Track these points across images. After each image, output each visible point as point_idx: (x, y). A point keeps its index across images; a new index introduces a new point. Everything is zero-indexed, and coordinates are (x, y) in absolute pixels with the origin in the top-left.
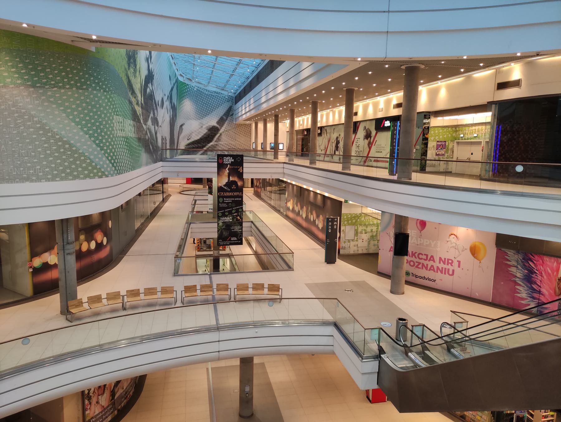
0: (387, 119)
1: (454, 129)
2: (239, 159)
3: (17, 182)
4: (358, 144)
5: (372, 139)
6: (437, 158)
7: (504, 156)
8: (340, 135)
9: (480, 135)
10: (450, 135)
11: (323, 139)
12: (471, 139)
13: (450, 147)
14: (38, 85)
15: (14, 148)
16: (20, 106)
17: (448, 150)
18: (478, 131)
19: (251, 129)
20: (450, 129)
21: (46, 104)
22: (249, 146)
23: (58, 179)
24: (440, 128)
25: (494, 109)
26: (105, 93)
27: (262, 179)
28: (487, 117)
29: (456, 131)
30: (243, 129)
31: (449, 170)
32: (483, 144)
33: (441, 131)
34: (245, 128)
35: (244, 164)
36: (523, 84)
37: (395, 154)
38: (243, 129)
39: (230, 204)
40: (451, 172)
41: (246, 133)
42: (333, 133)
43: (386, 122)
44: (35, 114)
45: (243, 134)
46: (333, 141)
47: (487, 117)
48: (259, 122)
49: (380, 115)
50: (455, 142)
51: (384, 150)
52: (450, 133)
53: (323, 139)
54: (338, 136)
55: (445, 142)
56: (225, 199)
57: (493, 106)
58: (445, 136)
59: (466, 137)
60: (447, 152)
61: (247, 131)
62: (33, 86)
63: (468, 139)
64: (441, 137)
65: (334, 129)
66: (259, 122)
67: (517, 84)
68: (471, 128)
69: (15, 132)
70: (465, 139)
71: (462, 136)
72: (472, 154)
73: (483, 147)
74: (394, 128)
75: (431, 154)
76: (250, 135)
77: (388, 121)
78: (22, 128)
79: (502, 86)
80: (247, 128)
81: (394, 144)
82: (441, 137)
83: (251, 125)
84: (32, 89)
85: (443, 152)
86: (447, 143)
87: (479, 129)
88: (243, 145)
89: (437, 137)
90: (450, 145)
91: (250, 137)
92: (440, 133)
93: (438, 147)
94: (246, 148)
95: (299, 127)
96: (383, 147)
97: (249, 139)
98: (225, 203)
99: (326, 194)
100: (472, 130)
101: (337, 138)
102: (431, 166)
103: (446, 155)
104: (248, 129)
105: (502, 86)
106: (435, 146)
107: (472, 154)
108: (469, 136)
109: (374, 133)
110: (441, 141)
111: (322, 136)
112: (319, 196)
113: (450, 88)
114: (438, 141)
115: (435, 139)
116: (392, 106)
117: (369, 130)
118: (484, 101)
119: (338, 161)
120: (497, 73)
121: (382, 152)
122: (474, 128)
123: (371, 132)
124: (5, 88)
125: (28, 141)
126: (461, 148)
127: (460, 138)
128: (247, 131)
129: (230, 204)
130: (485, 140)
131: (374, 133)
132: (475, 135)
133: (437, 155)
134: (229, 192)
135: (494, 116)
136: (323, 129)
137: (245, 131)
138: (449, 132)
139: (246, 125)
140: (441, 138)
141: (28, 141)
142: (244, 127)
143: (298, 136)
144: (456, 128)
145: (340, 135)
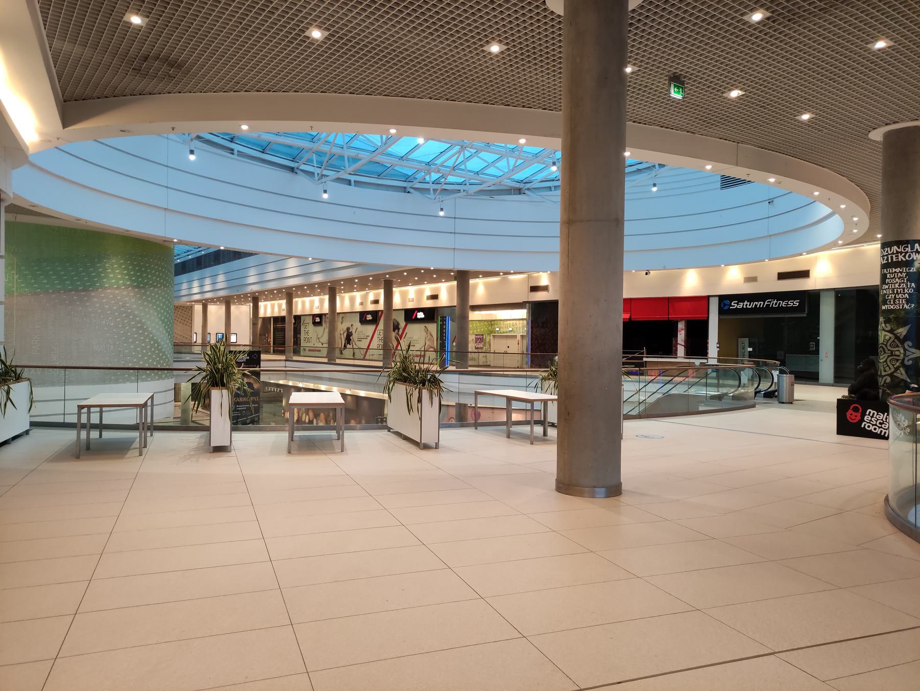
0: (420, 310)
1: (489, 322)
2: (256, 356)
3: (120, 383)
4: (307, 330)
5: (401, 331)
6: (476, 351)
7: (539, 349)
8: (352, 325)
9: (515, 329)
10: (486, 329)
11: (325, 329)
12: (506, 332)
13: (487, 340)
14: (141, 285)
15: (120, 348)
16: (127, 306)
17: (485, 343)
18: (513, 325)
19: (192, 314)
20: (486, 322)
21: (145, 303)
22: (189, 338)
23: (149, 379)
24: (477, 322)
25: (402, 185)
26: (166, 289)
27: (623, 349)
28: (523, 313)
29: (492, 325)
30: (179, 313)
31: (488, 364)
32: (519, 338)
33: (478, 324)
34: (183, 312)
35: (261, 362)
36: (550, 289)
37: (759, 361)
38: (179, 313)
39: (244, 412)
40: (490, 365)
41: (184, 318)
42: (342, 323)
43: (418, 314)
44: (137, 314)
45: (180, 320)
46: (342, 332)
47: (523, 313)
48: (209, 304)
49: (410, 306)
50: (491, 336)
51: (417, 343)
52: (486, 327)
53: (325, 329)
54: (350, 326)
55: (483, 335)
56: (237, 406)
57: (527, 304)
58: (482, 330)
59: (502, 330)
60: (485, 345)
61: (185, 316)
62: (138, 287)
63: (504, 333)
64: (479, 330)
65: (343, 318)
66: (209, 304)
67: (545, 288)
68: (505, 323)
69: (122, 332)
70: (501, 333)
71: (498, 329)
72: (508, 347)
73: (518, 341)
74: (443, 323)
75: (471, 347)
76: (190, 322)
77: (421, 313)
78: (127, 328)
79: (534, 289)
80: (185, 311)
81: (444, 338)
82: (479, 330)
83: (191, 307)
84: (137, 290)
85: (481, 345)
86: (484, 336)
87: (513, 323)
88: (178, 337)
89: (475, 331)
90: (487, 338)
91: (190, 325)
92: (477, 326)
93: (477, 340)
94: (185, 341)
95: (280, 311)
96: (416, 341)
97: (190, 328)
98: (238, 411)
99: (362, 393)
100: (507, 324)
101: (348, 329)
102: (472, 360)
103: (484, 348)
104: (187, 313)
105: (534, 289)
106: (474, 340)
107: (508, 347)
108: (505, 330)
109: (402, 324)
110: (479, 335)
111: (322, 325)
112: (349, 398)
113: (487, 286)
114: (476, 335)
115: (473, 332)
116: (425, 298)
117: (396, 321)
118: (520, 301)
119: (352, 357)
120: (529, 277)
121: (414, 346)
122: (508, 322)
123: (398, 324)
124: (118, 289)
125: (131, 340)
126: (497, 341)
127: (496, 332)
128: (185, 316)
129: (244, 412)
130: (520, 334)
131: (402, 324)
132: (511, 329)
133: (476, 348)
134: (243, 397)
135: (528, 313)
136: (324, 317)
137: (183, 317)
138: (485, 325)
139: (184, 307)
140: (479, 331)
141: (131, 340)
142: (180, 310)
143: (276, 324)
144: (492, 322)
145: (352, 325)
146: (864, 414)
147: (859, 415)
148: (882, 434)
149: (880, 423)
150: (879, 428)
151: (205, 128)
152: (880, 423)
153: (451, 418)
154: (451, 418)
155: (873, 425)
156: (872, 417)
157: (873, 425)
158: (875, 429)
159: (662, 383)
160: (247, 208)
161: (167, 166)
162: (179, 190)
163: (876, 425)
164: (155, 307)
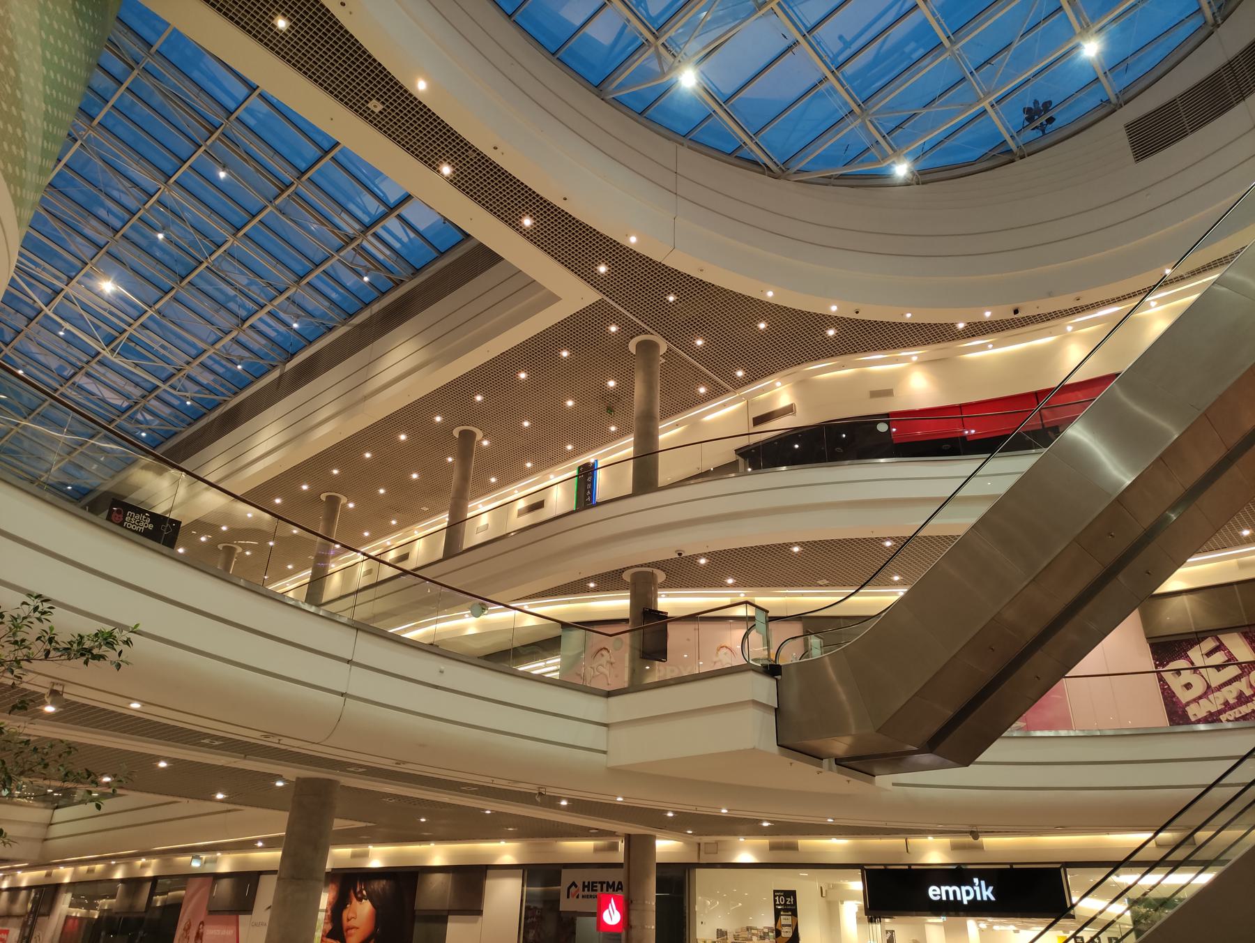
36: (797, 409)
67: (789, 410)
146: (125, 516)
147: (121, 516)
148: (952, 898)
149: (138, 522)
150: (137, 526)
151: (1185, 901)
152: (138, 522)
153: (601, 649)
154: (601, 649)
155: (133, 524)
156: (131, 518)
157: (133, 524)
158: (134, 527)
159: (1220, 861)
160: (151, 821)
161: (349, 662)
162: (498, 44)
163: (134, 524)
164: (292, 585)
